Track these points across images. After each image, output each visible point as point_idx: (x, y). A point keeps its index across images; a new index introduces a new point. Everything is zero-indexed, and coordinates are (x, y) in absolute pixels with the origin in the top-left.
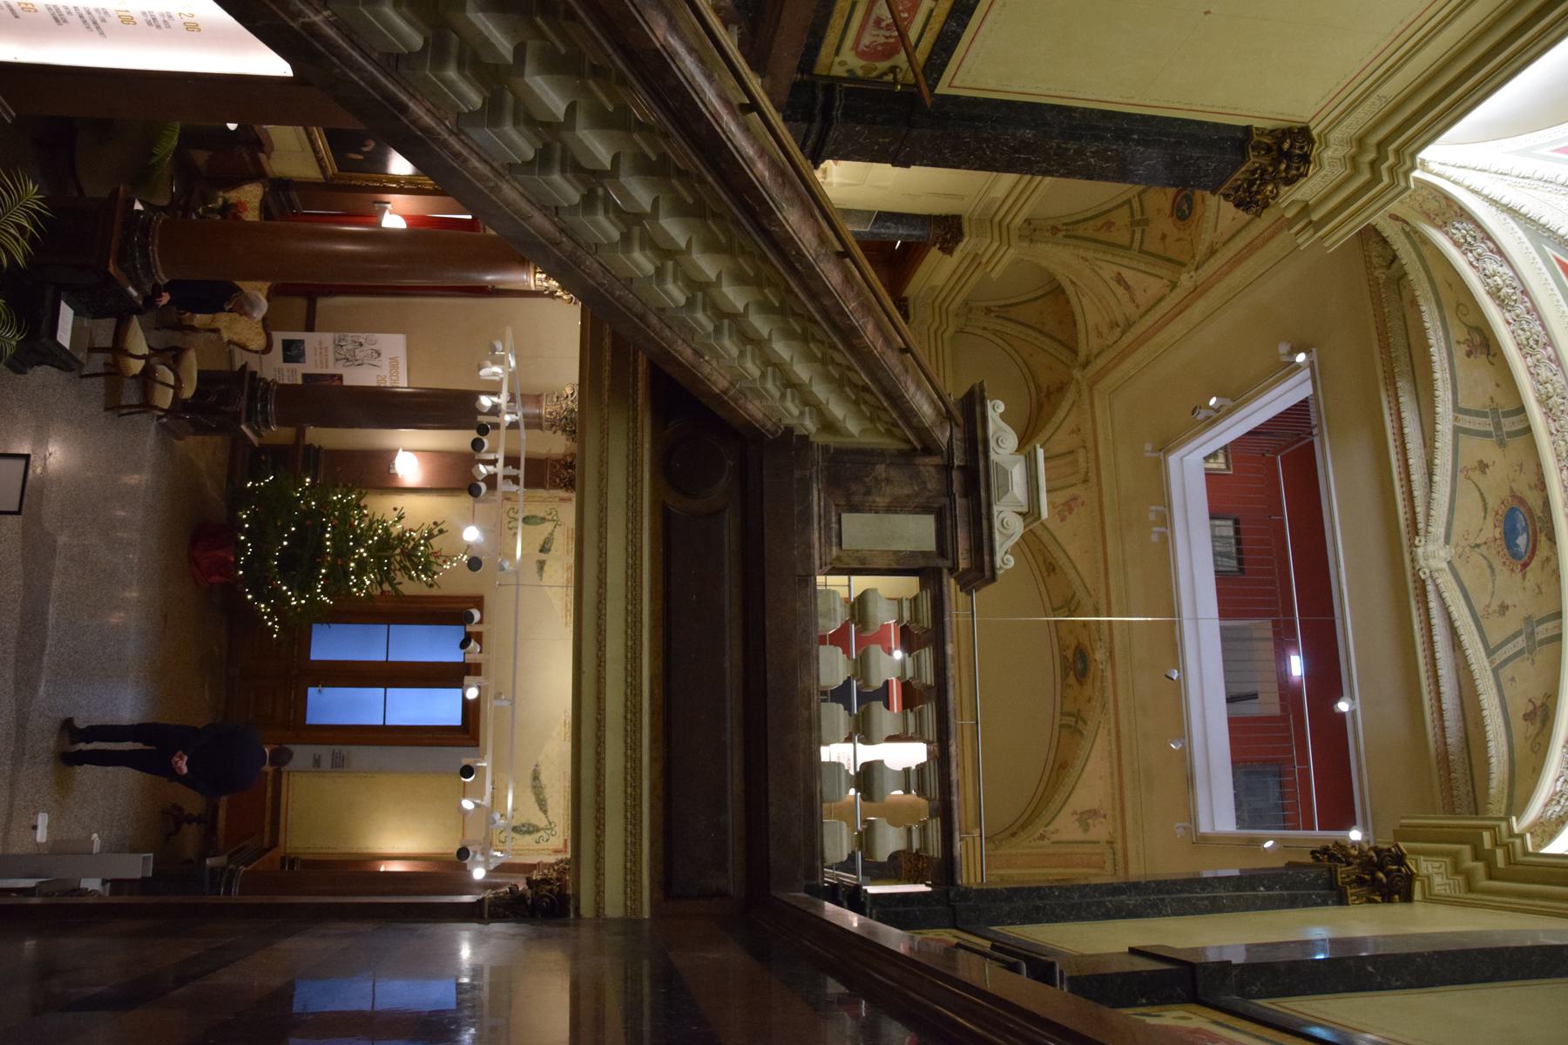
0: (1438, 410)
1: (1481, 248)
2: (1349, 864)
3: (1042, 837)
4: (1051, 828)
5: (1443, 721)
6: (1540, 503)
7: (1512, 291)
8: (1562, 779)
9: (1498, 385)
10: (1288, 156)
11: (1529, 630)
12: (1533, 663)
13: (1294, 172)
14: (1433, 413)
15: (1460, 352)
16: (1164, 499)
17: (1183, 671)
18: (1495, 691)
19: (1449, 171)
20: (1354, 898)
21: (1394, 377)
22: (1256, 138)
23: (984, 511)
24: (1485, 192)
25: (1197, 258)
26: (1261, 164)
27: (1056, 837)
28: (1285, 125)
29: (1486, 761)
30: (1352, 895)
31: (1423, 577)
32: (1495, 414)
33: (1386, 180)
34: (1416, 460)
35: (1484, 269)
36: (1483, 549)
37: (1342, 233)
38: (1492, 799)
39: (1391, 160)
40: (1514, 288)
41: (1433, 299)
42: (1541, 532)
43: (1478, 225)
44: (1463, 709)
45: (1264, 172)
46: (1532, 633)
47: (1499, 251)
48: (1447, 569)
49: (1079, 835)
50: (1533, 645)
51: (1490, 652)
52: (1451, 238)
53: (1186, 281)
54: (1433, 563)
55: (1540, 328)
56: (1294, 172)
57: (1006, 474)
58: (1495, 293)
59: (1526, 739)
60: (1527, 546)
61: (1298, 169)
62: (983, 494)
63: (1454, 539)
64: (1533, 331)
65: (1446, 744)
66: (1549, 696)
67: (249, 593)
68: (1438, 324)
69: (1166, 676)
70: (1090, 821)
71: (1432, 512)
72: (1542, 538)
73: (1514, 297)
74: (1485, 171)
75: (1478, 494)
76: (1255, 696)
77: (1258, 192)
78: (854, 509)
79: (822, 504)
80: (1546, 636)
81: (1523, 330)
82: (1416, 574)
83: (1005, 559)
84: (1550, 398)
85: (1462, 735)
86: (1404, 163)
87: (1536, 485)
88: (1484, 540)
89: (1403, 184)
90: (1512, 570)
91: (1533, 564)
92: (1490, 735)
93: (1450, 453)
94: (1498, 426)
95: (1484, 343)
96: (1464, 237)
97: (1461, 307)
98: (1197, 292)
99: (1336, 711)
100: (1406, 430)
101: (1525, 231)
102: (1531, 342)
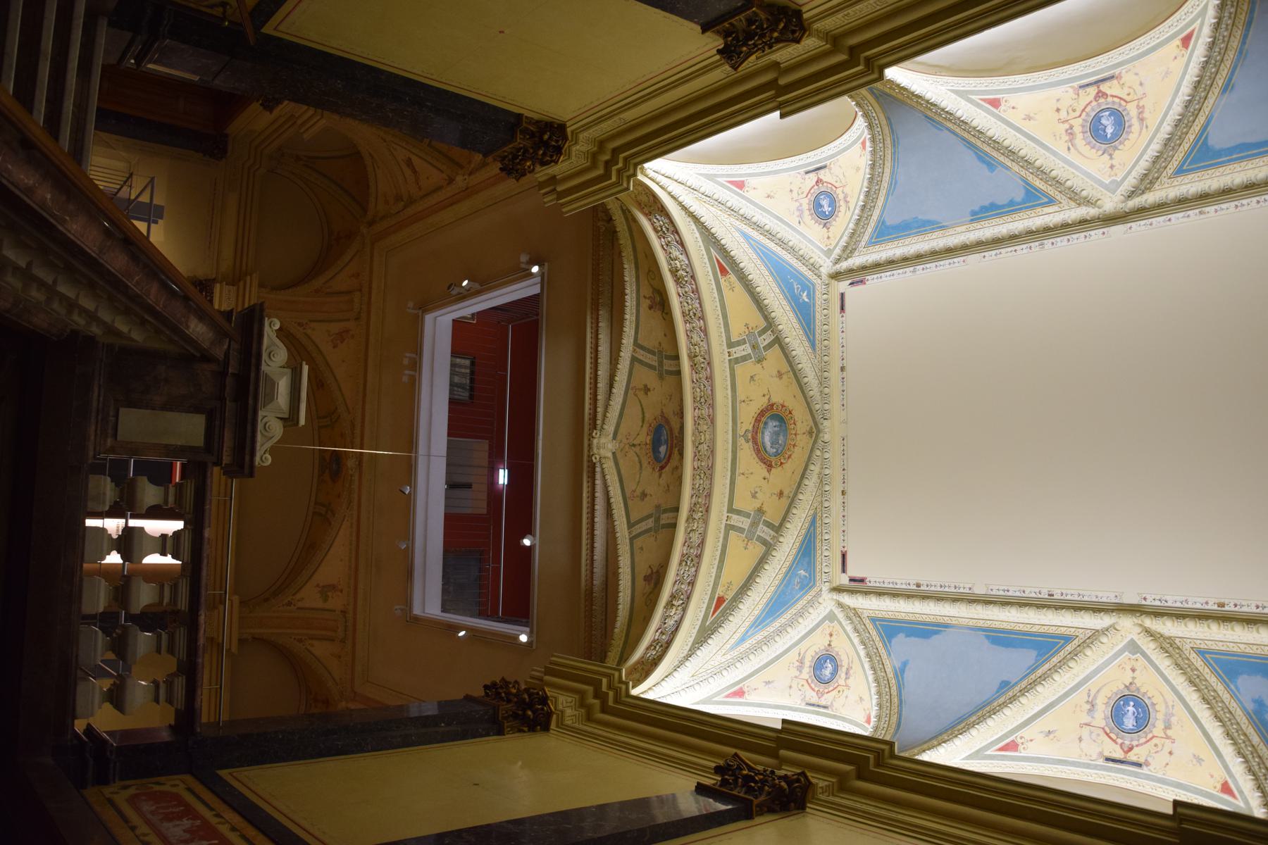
0: (624, 341)
1: (671, 237)
2: (509, 701)
3: (289, 604)
4: (298, 596)
5: (593, 568)
6: (678, 426)
7: (685, 274)
8: (660, 631)
9: (665, 335)
10: (546, 144)
11: (657, 515)
12: (656, 541)
13: (548, 158)
14: (620, 344)
15: (645, 303)
16: (417, 348)
17: (414, 488)
18: (629, 555)
19: (659, 178)
20: (509, 729)
21: (598, 305)
22: (524, 125)
23: (250, 417)
24: (680, 199)
25: (472, 166)
26: (524, 145)
27: (300, 605)
28: (546, 119)
29: (614, 621)
30: (508, 727)
31: (594, 461)
32: (660, 354)
33: (614, 179)
34: (603, 372)
35: (670, 253)
36: (637, 449)
37: (575, 206)
38: (615, 636)
39: (620, 165)
40: (687, 273)
41: (633, 261)
42: (676, 447)
43: (672, 222)
44: (607, 561)
45: (526, 151)
46: (659, 517)
47: (682, 244)
48: (612, 458)
49: (320, 604)
50: (658, 527)
51: (630, 525)
52: (652, 224)
53: (460, 181)
54: (603, 452)
55: (698, 306)
56: (548, 158)
57: (272, 385)
58: (674, 272)
59: (644, 595)
60: (666, 454)
61: (552, 156)
62: (251, 401)
63: (619, 437)
64: (694, 306)
65: (592, 584)
66: (662, 567)
68: (634, 280)
69: (401, 491)
70: (329, 594)
71: (608, 415)
72: (676, 451)
73: (686, 279)
74: (683, 184)
75: (640, 408)
76: (469, 486)
77: (519, 163)
78: (132, 404)
79: (101, 399)
80: (667, 522)
81: (687, 303)
82: (590, 456)
83: (263, 458)
85: (604, 579)
86: (629, 170)
87: (678, 414)
88: (639, 442)
89: (625, 185)
90: (653, 469)
91: (667, 469)
92: (621, 588)
94: (661, 364)
95: (660, 302)
96: (661, 227)
97: (651, 273)
98: (469, 192)
99: (522, 544)
100: (600, 348)
101: (701, 234)
102: (691, 314)
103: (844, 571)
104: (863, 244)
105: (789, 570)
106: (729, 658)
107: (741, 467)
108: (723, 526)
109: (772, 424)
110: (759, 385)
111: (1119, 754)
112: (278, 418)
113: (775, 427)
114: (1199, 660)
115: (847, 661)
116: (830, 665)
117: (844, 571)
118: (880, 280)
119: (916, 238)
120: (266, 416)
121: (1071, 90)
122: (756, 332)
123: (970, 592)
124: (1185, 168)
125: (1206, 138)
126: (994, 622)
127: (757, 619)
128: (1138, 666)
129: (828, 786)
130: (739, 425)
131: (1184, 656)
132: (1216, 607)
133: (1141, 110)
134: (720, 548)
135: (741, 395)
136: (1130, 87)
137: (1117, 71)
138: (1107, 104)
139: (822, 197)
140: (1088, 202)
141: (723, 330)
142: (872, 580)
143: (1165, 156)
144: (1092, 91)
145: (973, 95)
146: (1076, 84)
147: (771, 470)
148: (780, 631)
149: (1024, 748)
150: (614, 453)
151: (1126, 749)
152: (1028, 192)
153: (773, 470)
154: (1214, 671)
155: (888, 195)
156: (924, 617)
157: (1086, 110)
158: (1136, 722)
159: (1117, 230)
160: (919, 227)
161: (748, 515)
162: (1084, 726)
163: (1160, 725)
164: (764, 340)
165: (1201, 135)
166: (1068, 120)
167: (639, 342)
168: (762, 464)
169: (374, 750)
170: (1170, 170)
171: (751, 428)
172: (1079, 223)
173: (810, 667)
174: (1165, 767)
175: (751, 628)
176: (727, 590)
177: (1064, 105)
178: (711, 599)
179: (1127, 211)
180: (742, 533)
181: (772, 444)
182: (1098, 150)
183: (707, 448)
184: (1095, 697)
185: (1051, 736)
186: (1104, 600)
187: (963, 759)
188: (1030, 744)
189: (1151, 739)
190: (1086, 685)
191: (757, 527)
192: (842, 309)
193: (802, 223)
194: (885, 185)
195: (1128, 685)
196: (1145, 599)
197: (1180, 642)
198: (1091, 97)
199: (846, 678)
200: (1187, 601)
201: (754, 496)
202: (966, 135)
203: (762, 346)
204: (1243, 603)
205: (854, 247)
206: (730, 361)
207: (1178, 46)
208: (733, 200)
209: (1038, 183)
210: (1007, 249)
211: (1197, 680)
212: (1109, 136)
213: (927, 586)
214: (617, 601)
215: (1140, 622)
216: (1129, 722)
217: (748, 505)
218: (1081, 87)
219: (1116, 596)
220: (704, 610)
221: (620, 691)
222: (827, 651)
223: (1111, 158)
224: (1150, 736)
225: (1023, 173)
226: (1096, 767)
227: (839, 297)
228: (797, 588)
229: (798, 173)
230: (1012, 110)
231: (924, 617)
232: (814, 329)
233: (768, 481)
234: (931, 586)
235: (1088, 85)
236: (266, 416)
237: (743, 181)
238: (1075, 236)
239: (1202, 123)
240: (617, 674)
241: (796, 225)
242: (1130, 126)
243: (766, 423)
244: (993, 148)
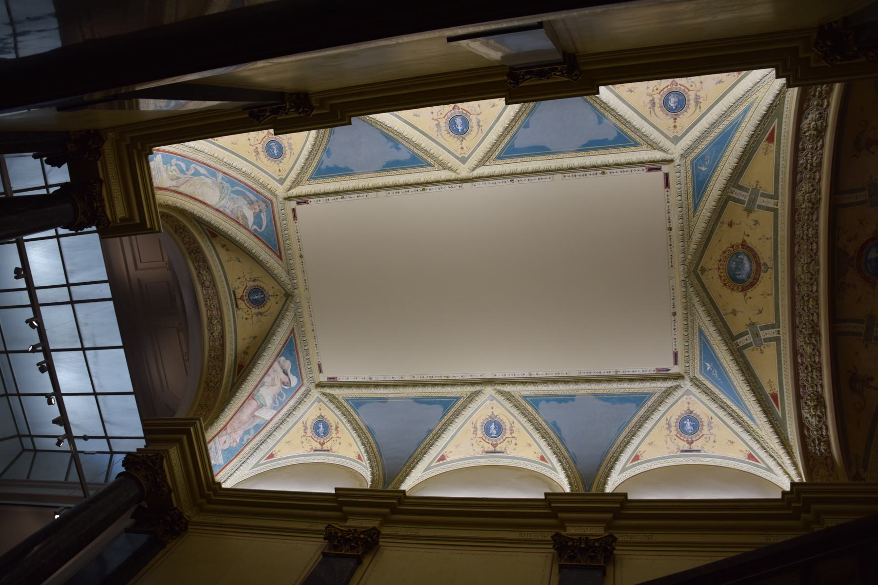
7: (808, 402)
73: (809, 398)
84: (809, 334)
101: (786, 430)
102: (810, 369)
103: (667, 176)
104: (657, 395)
107: (770, 244)
108: (780, 198)
109: (743, 276)
110: (755, 306)
113: (740, 274)
115: (656, 111)
116: (672, 105)
118: (644, 370)
119: (615, 392)
123: (564, 175)
124: (455, 400)
125: (444, 411)
128: (460, 151)
132: (426, 188)
133: (475, 432)
135: (771, 300)
136: (479, 445)
137: (484, 454)
139: (690, 432)
140: (501, 393)
141: (782, 352)
142: (642, 172)
144: (694, 446)
145: (764, 468)
146: (505, 455)
147: (743, 242)
148: (714, 125)
151: (456, 107)
152: (537, 405)
153: (740, 242)
154: (421, 157)
155: (629, 422)
156: (597, 153)
157: (503, 440)
159: (488, 376)
160: (612, 398)
161: (760, 207)
163: (442, 124)
164: (747, 340)
165: (445, 414)
168: (751, 247)
171: (762, 274)
173: (689, 100)
177: (512, 446)
180: (762, 193)
181: (742, 262)
183: (801, 260)
184: (478, 129)
185: (492, 105)
186: (481, 183)
189: (445, 116)
191: (750, 198)
195: (464, 140)
196: (460, 187)
198: (499, 446)
199: (653, 100)
200: (439, 189)
201: (756, 222)
202: (561, 446)
203: (750, 335)
206: (779, 327)
207: (448, 457)
209: (530, 408)
212: (493, 424)
213: (596, 174)
216: (459, 121)
217: (758, 214)
218: (503, 452)
220: (783, 131)
222: (677, 115)
224: (446, 118)
225: (537, 416)
229: (705, 452)
231: (597, 153)
232: (701, 344)
233: (744, 234)
234: (583, 175)
235: (499, 452)
238: (511, 376)
242: (482, 426)
243: (749, 277)
244: (548, 434)
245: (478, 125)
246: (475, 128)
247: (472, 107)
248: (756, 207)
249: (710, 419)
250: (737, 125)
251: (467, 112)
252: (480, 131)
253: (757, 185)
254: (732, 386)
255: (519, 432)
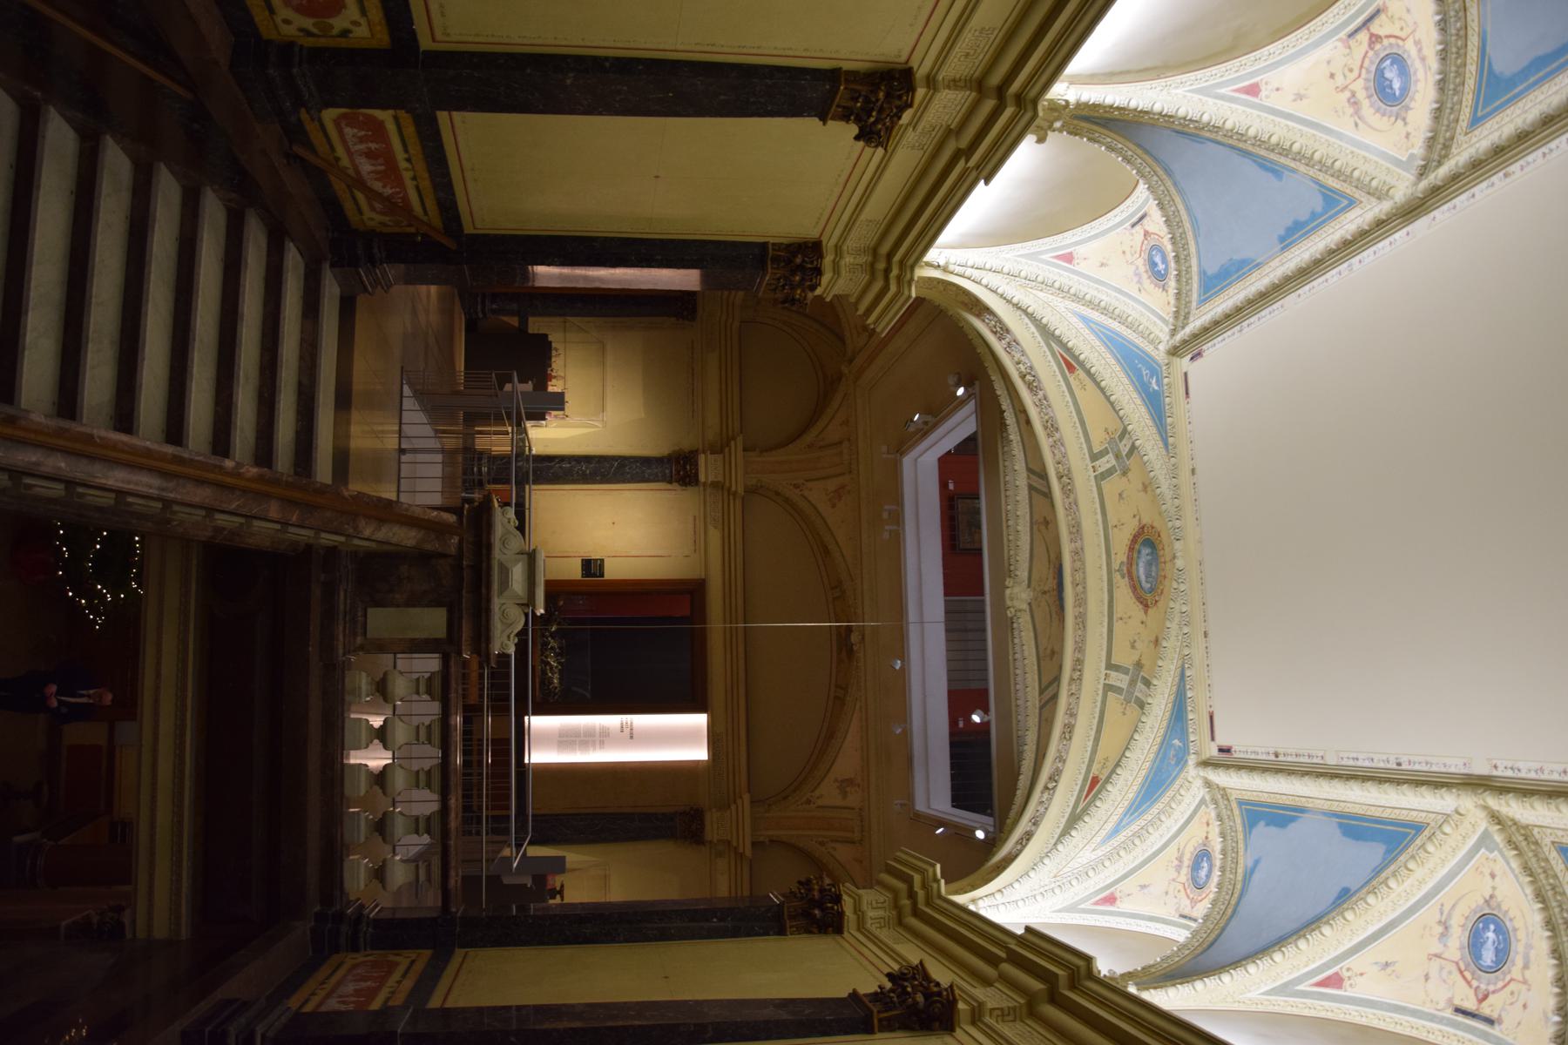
3: (809, 802)
4: (817, 793)
19: (969, 272)
27: (820, 802)
54: (1016, 603)
57: (505, 572)
67: (69, 591)
70: (848, 789)
79: (348, 601)
93: (1028, 506)
104: (1194, 304)
105: (1164, 740)
106: (1100, 854)
107: (1119, 610)
108: (1101, 687)
111: (1470, 1005)
112: (518, 604)
114: (1560, 861)
117: (1213, 739)
120: (504, 604)
121: (1339, 44)
122: (1116, 437)
123: (1321, 762)
126: (1348, 805)
127: (1132, 805)
129: (1014, 1009)
130: (1113, 556)
131: (1542, 856)
134: (1097, 715)
135: (1112, 520)
138: (1385, 49)
139: (1154, 253)
141: (1083, 440)
143: (1449, 105)
146: (1343, 34)
149: (1351, 985)
150: (1030, 604)
151: (1480, 996)
153: (1150, 610)
155: (1196, 237)
158: (1496, 956)
160: (1238, 270)
161: (1125, 671)
162: (1434, 958)
166: (1346, 87)
167: (1030, 466)
169: (627, 941)
170: (1463, 124)
171: (1125, 560)
172: (1378, 226)
174: (1517, 1027)
175: (1125, 815)
176: (1103, 768)
178: (1085, 780)
179: (1421, 196)
181: (1147, 577)
182: (1390, 117)
184: (1449, 916)
185: (1389, 970)
186: (1453, 770)
187: (1263, 994)
188: (1359, 980)
190: (1436, 899)
192: (1187, 393)
193: (1142, 290)
194: (1187, 225)
195: (1488, 898)
196: (1496, 767)
197: (1539, 833)
200: (1542, 770)
204: (1416, 760)
205: (1186, 310)
206: (1096, 477)
208: (1061, 276)
210: (1331, 272)
211: (1550, 893)
212: (1397, 93)
214: (1016, 784)
215: (1482, 803)
216: (1488, 956)
217: (1123, 657)
219: (1465, 764)
221: (932, 890)
223: (1406, 124)
226: (1441, 1020)
227: (1183, 375)
228: (1173, 763)
230: (1276, 92)
236: (504, 604)
237: (1071, 253)
239: (1476, 44)
240: (931, 870)
241: (1135, 294)
243: (1139, 552)
245: (1446, 928)
246: (1456, 921)
247: (1444, 981)
248: (1131, 671)
249: (1142, 289)
250: (1131, 811)
251: (1461, 972)
252: (1446, 909)
253: (1125, 708)
254: (1122, 361)
255: (1336, 112)
